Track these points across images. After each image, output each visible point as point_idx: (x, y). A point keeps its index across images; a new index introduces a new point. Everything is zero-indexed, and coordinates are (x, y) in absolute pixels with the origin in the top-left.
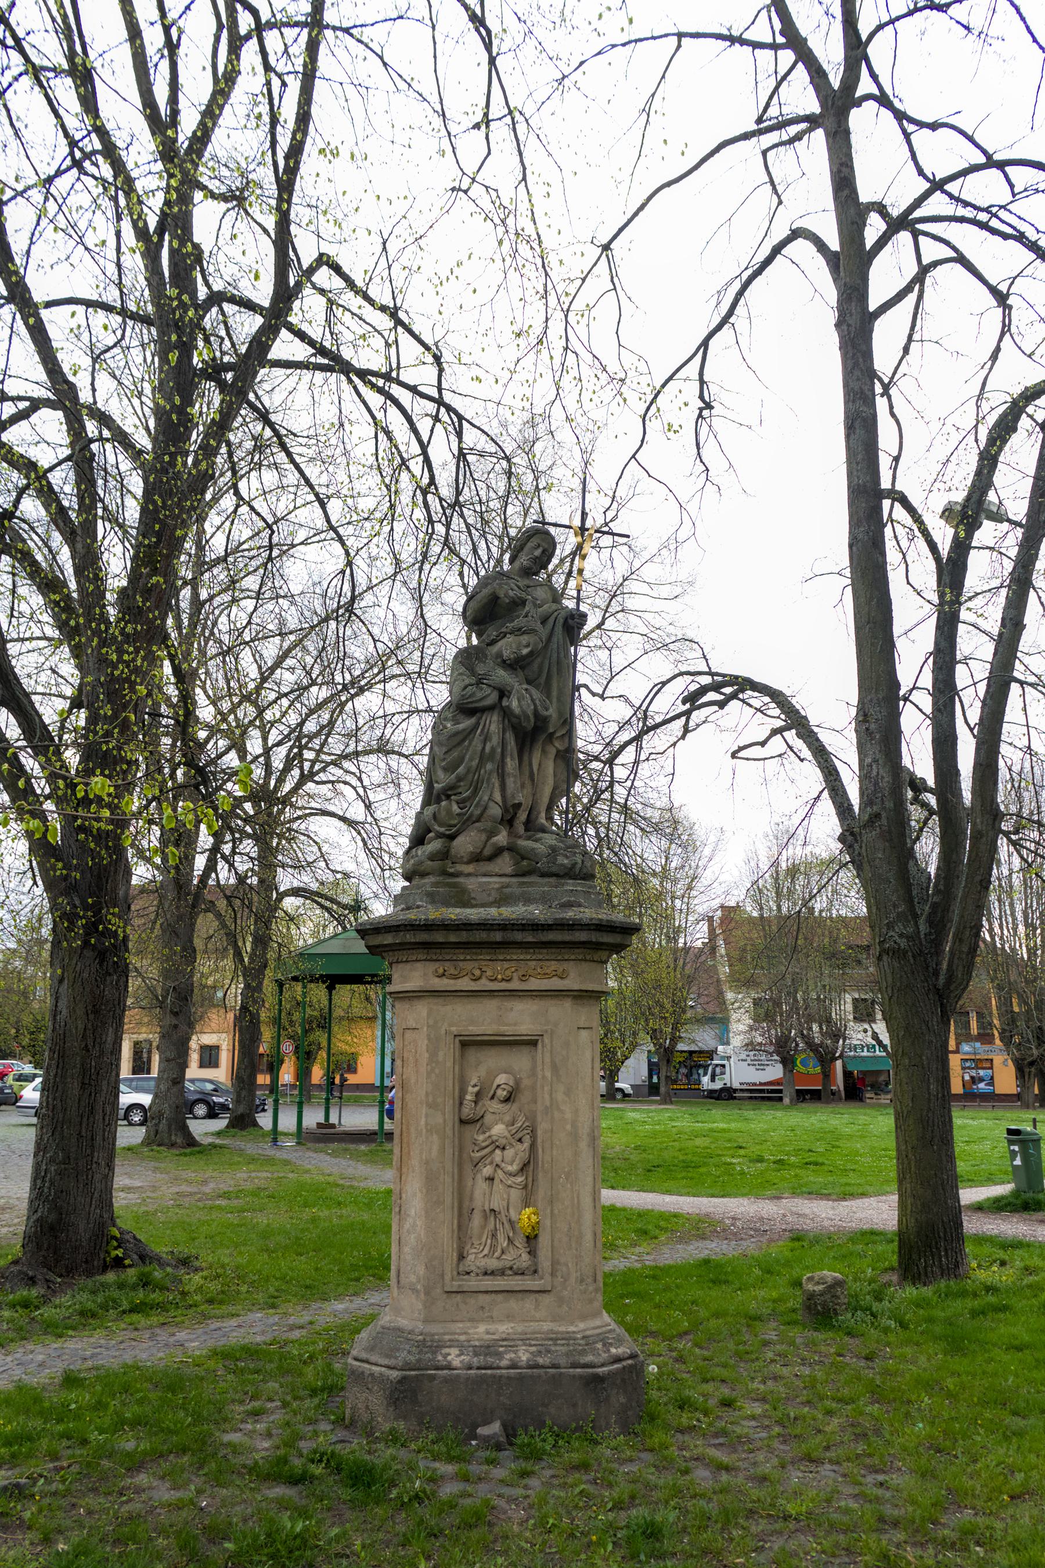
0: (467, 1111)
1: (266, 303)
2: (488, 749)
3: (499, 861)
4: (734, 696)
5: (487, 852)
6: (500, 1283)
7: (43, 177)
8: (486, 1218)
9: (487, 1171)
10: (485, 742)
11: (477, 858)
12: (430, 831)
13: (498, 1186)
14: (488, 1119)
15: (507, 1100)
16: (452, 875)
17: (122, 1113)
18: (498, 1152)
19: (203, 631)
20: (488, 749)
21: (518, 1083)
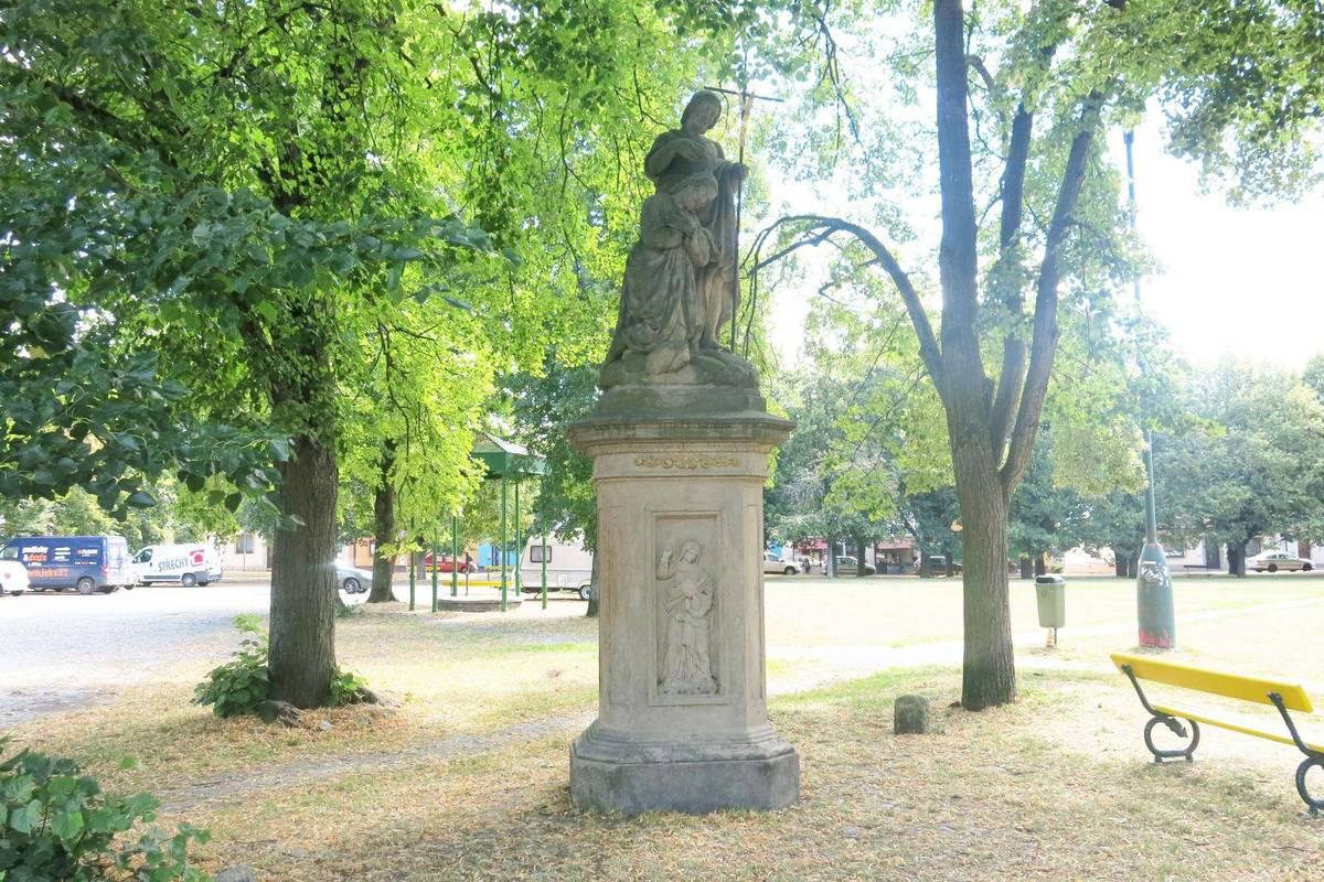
0: (664, 570)
1: (948, 594)
2: (674, 282)
3: (682, 372)
4: (824, 236)
5: (676, 365)
6: (689, 700)
7: (1113, 571)
8: (679, 651)
9: (678, 616)
10: (672, 275)
11: (666, 371)
12: (626, 348)
13: (688, 628)
14: (679, 576)
15: (692, 562)
16: (646, 384)
17: (341, 584)
18: (687, 601)
19: (94, 403)
20: (674, 282)
21: (702, 548)
